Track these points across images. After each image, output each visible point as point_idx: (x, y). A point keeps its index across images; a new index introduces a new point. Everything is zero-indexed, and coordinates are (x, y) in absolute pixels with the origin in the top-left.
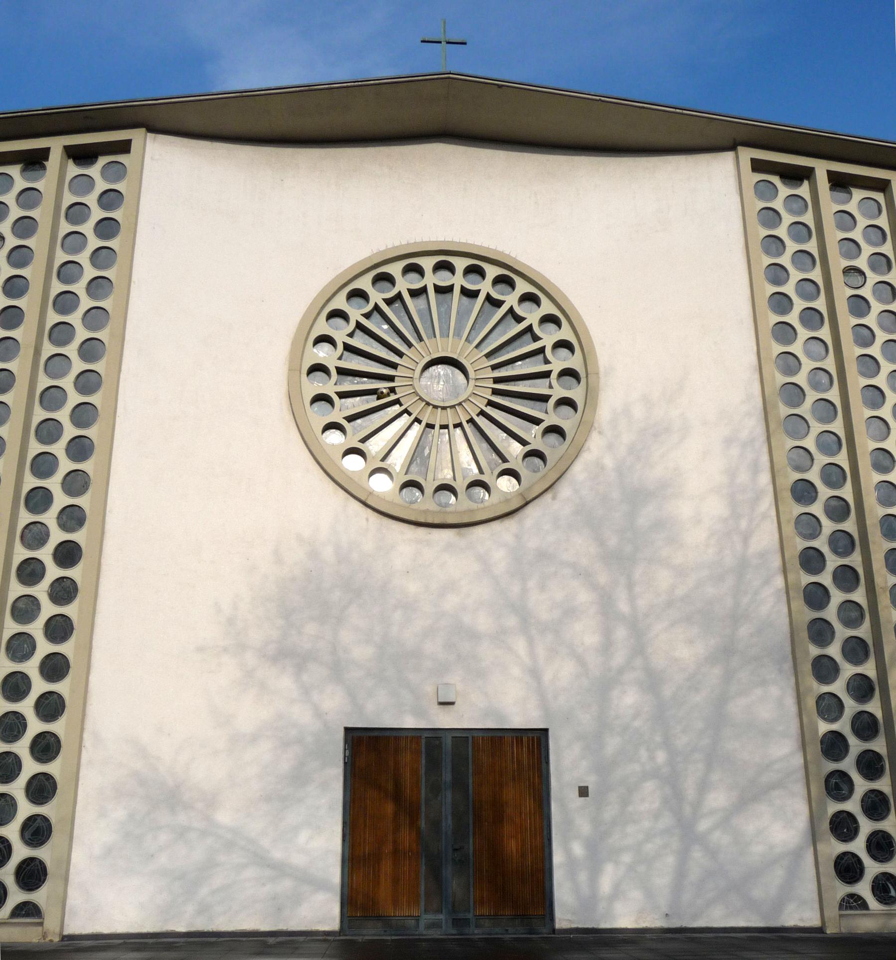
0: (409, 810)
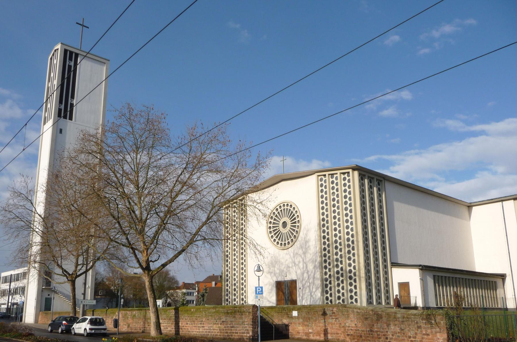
0: (284, 294)
